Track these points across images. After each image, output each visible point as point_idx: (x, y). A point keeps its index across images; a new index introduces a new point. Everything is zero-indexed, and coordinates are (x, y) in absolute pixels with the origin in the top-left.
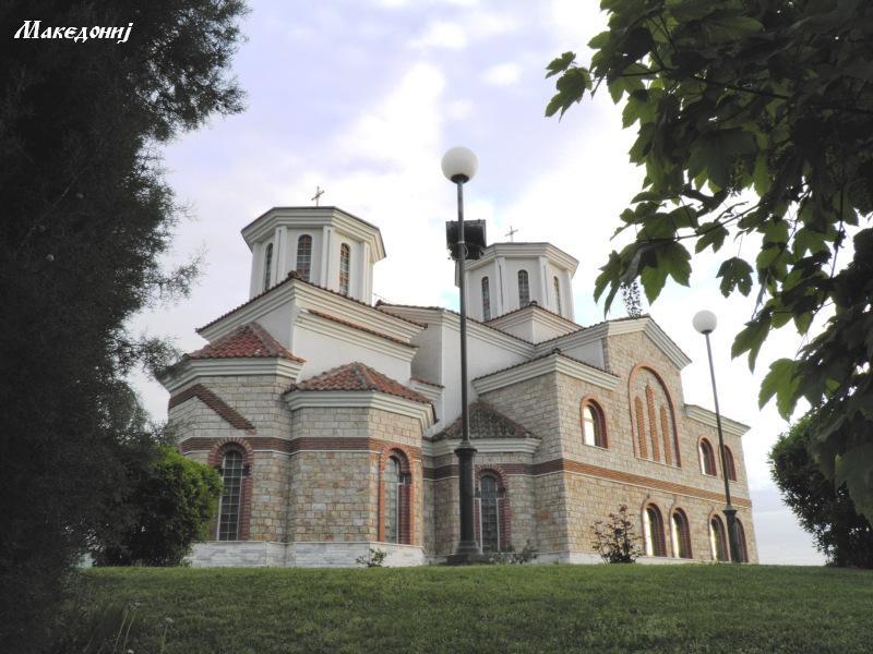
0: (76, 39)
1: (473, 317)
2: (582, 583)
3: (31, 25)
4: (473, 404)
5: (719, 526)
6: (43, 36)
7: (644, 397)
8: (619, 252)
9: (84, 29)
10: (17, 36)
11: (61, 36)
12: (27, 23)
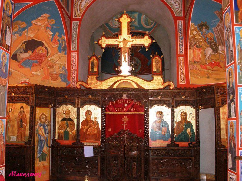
0: (26, 176)
1: (49, 174)
2: (45, 94)
3: (14, 172)
4: (178, 123)
5: (230, 144)
6: (17, 176)
7: (76, 119)
8: (61, 144)
9: (28, 174)
10: (10, 176)
11: (22, 176)
12: (12, 172)
